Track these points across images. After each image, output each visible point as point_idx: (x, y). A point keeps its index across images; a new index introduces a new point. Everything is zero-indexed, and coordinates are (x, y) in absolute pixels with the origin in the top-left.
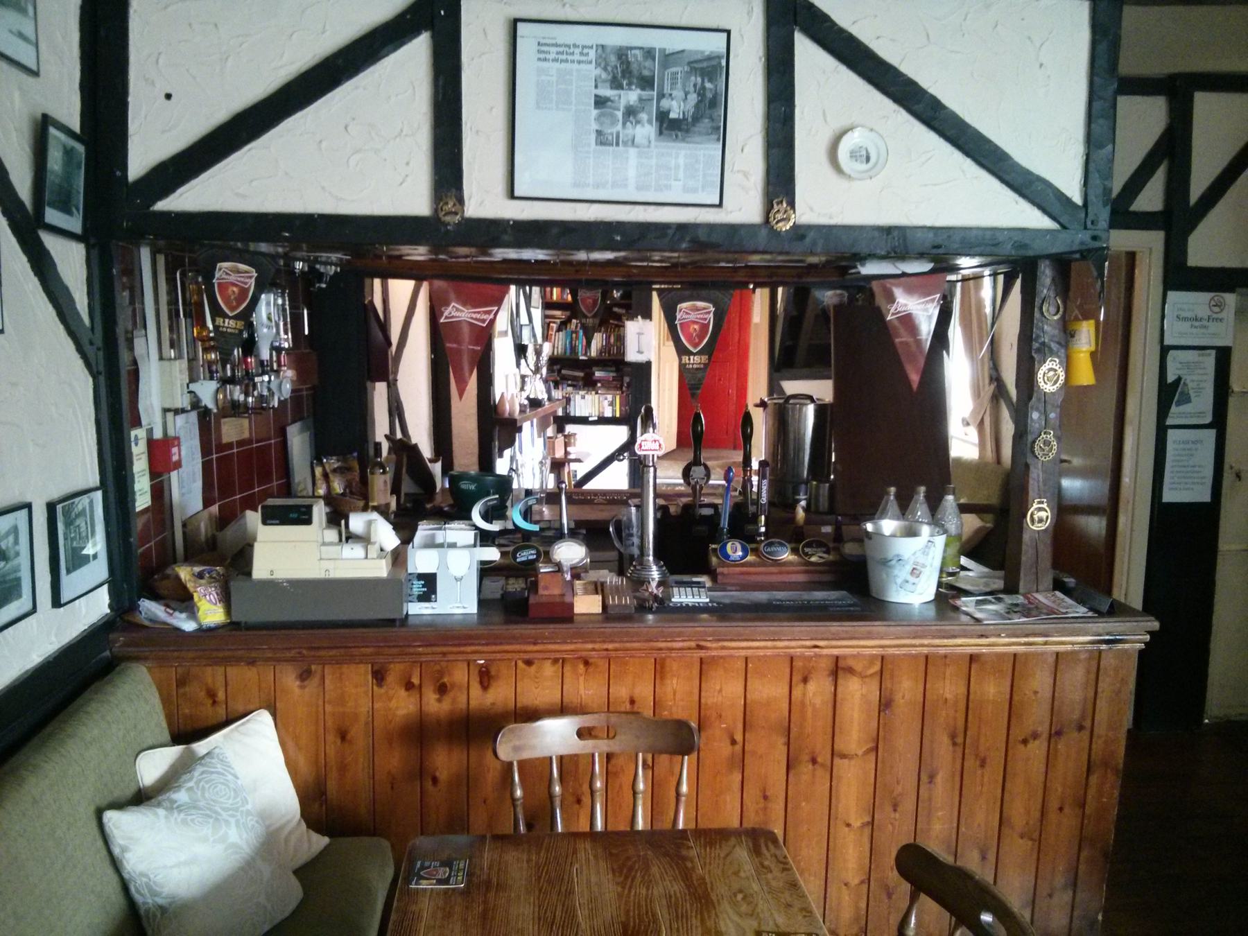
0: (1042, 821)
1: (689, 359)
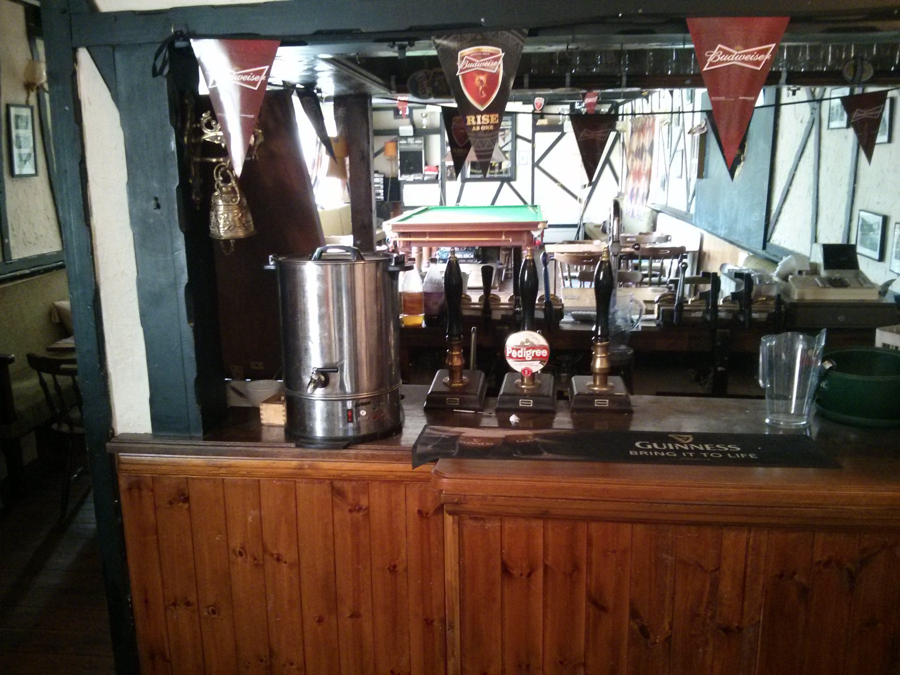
0: (302, 622)
1: (476, 120)
